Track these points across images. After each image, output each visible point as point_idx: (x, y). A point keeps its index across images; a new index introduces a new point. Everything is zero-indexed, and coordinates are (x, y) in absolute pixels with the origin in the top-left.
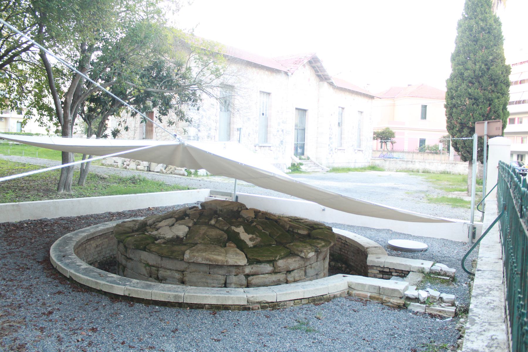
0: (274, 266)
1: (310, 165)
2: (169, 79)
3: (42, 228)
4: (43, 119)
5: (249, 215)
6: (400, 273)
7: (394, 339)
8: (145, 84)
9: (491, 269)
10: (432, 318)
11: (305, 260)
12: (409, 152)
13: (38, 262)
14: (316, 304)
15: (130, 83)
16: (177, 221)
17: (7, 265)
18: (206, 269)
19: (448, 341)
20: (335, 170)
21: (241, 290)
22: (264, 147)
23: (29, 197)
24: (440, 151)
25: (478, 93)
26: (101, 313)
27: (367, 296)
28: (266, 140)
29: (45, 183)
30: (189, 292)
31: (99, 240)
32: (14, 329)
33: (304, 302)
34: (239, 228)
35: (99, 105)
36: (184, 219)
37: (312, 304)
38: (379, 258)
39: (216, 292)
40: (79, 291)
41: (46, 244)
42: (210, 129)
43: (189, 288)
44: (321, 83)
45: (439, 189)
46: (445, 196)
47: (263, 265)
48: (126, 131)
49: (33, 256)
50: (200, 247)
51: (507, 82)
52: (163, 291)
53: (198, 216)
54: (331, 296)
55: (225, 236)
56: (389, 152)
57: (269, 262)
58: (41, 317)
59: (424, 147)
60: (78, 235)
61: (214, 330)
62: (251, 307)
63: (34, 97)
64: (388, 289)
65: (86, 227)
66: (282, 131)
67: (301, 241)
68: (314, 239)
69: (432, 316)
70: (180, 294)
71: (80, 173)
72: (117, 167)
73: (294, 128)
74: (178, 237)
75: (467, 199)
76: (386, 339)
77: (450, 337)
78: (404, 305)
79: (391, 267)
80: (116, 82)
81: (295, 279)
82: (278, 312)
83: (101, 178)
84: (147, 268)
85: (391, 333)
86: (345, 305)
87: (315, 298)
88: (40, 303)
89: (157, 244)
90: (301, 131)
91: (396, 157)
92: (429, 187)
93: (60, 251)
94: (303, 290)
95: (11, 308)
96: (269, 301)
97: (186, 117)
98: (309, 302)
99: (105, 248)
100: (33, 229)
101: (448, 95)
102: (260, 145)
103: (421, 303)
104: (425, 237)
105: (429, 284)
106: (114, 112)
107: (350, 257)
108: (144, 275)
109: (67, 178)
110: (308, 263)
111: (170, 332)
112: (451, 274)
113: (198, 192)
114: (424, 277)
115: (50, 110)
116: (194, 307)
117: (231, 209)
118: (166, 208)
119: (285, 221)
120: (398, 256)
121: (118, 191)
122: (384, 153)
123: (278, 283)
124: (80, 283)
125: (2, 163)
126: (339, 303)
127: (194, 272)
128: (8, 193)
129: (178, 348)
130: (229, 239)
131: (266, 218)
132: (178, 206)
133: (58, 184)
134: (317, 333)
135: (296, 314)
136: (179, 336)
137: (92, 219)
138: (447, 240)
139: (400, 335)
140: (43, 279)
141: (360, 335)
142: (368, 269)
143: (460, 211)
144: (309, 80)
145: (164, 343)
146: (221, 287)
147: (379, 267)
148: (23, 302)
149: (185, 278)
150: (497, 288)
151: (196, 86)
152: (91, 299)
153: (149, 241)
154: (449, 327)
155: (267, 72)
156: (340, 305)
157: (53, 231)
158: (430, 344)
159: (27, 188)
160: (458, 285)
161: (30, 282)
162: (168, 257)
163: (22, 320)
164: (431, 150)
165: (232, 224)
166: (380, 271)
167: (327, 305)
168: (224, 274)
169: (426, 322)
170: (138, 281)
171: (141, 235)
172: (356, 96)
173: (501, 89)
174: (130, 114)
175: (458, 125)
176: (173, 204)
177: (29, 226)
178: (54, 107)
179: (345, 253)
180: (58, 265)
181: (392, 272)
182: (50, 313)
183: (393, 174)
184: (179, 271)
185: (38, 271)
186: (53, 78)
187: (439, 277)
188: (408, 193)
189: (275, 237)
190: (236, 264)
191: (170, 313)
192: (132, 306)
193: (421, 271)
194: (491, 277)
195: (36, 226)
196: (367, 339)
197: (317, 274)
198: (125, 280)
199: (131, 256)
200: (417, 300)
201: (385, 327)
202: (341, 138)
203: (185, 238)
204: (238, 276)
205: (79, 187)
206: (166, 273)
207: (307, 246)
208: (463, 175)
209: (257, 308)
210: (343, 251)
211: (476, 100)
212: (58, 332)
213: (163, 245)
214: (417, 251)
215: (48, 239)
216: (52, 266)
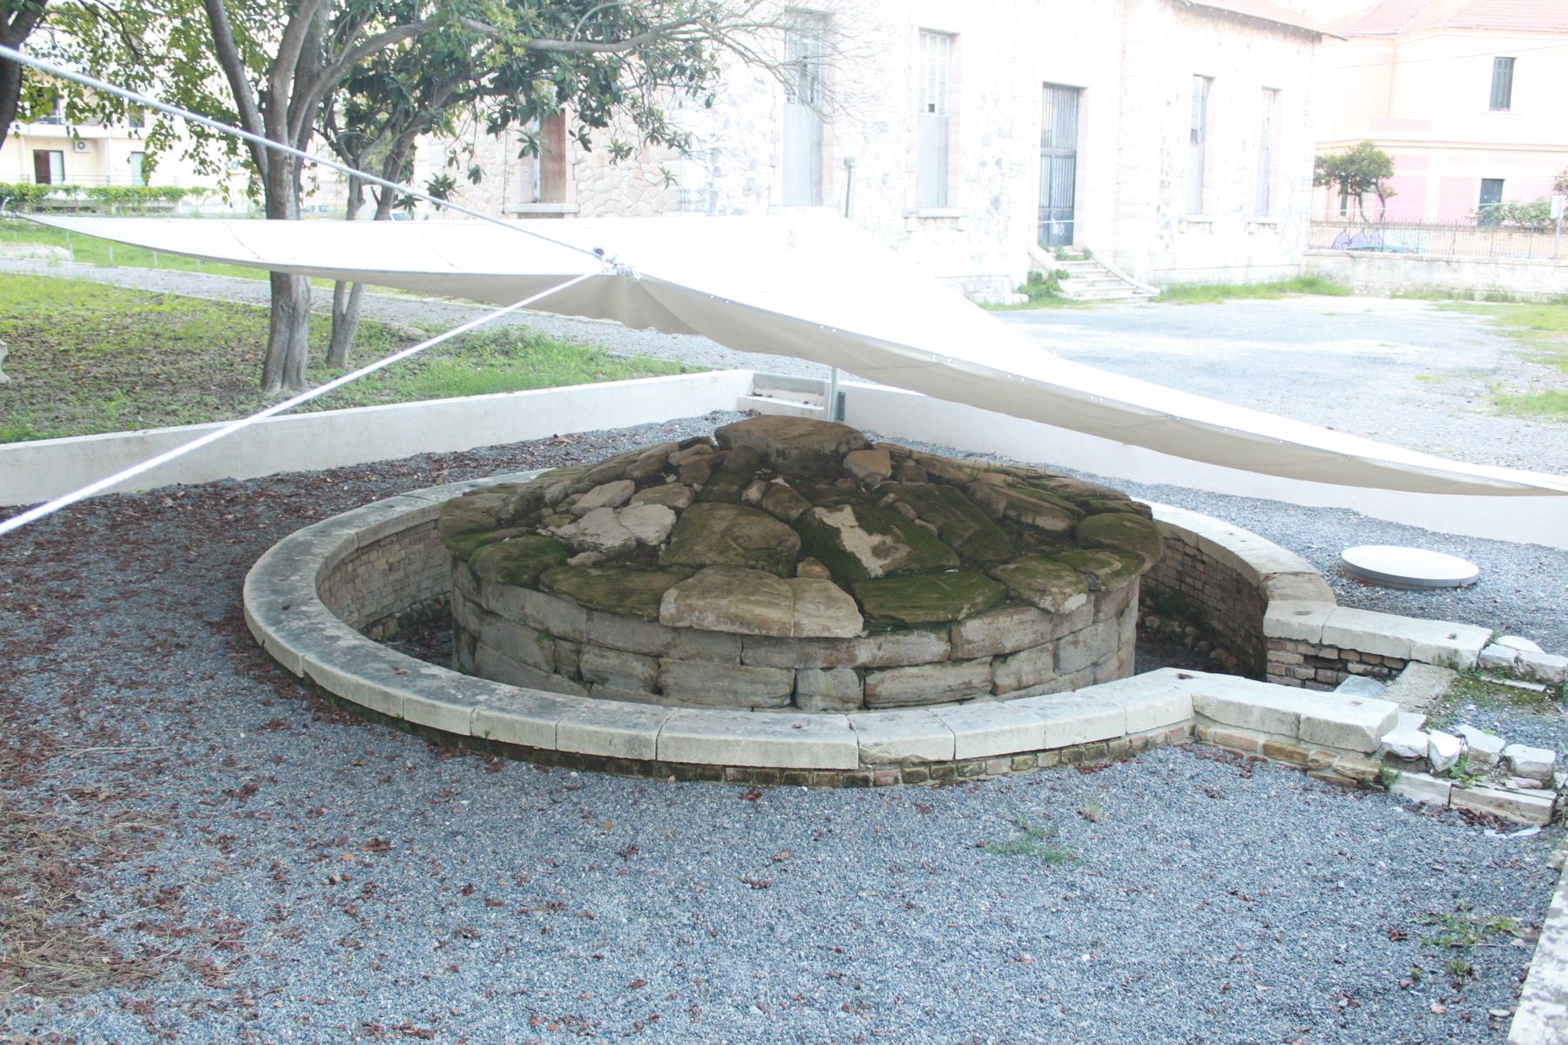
0: (950, 640)
1: (1091, 278)
3: (219, 511)
4: (206, 150)
5: (872, 469)
6: (1375, 665)
8: (526, 24)
10: (1472, 824)
11: (1055, 618)
12: (1438, 227)
13: (210, 624)
14: (1085, 768)
15: (479, 25)
16: (638, 489)
17: (117, 636)
18: (731, 648)
19: (1519, 908)
20: (1177, 293)
21: (841, 720)
22: (935, 218)
23: (174, 412)
24: (1553, 221)
26: (400, 792)
27: (1255, 743)
28: (943, 200)
29: (224, 360)
30: (673, 728)
31: (397, 547)
32: (144, 841)
33: (1043, 760)
34: (838, 514)
35: (383, 100)
36: (662, 482)
37: (1070, 767)
38: (1307, 613)
39: (758, 728)
40: (333, 721)
41: (232, 563)
42: (752, 167)
43: (675, 712)
45: (1540, 362)
47: (914, 637)
48: (475, 182)
49: (193, 603)
50: (712, 576)
52: (591, 723)
53: (708, 472)
54: (1134, 743)
55: (794, 540)
56: (1370, 226)
57: (935, 626)
58: (222, 803)
59: (1498, 209)
60: (329, 535)
61: (750, 852)
62: (871, 775)
64: (1328, 724)
66: (998, 163)
67: (1046, 557)
69: (1471, 818)
70: (645, 734)
73: (1038, 150)
74: (641, 544)
76: (1308, 892)
77: (1525, 894)
78: (1379, 779)
81: (1020, 681)
83: (401, 340)
84: (546, 643)
85: (1327, 873)
88: (217, 759)
89: (575, 567)
91: (1396, 244)
92: (1504, 353)
93: (275, 591)
94: (1042, 723)
96: (931, 756)
97: (670, 130)
98: (1060, 762)
99: (416, 573)
100: (193, 514)
102: (923, 213)
103: (1436, 775)
104: (1472, 539)
105: (1472, 707)
107: (1210, 603)
108: (537, 666)
109: (289, 346)
110: (1064, 630)
111: (613, 856)
112: (1551, 675)
113: (715, 380)
114: (1454, 684)
116: (691, 775)
117: (816, 447)
118: (612, 437)
119: (992, 486)
120: (1372, 606)
122: (1353, 232)
123: (962, 697)
124: (335, 696)
125: (93, 295)
126: (1160, 767)
127: (693, 657)
128: (110, 399)
129: (636, 909)
130: (807, 551)
131: (931, 478)
132: (650, 427)
134: (1081, 869)
136: (639, 871)
137: (374, 479)
138: (1550, 549)
140: (225, 680)
141: (1221, 879)
145: (592, 890)
146: (780, 707)
147: (1306, 642)
148: (168, 755)
151: (698, 26)
152: (370, 748)
153: (549, 559)
154: (1527, 860)
156: (1164, 772)
157: (251, 521)
158: (1455, 915)
163: (167, 813)
164: (1519, 220)
165: (815, 498)
166: (1306, 656)
167: (1121, 772)
168: (790, 664)
169: (1449, 839)
170: (514, 689)
171: (522, 540)
172: (1255, 33)
174: (484, 125)
177: (181, 506)
179: (1194, 587)
181: (1347, 661)
182: (249, 791)
183: (1381, 306)
184: (645, 655)
185: (212, 655)
187: (1508, 682)
188: (1426, 379)
189: (957, 544)
190: (826, 634)
191: (613, 792)
192: (497, 770)
193: (1449, 662)
195: (202, 506)
196: (1243, 891)
197: (1095, 664)
199: (494, 605)
200: (1422, 763)
201: (1309, 852)
203: (663, 546)
204: (834, 672)
206: (604, 661)
209: (890, 780)
210: (1189, 580)
212: (273, 852)
213: (594, 572)
214: (1441, 588)
215: (238, 549)
216: (252, 638)
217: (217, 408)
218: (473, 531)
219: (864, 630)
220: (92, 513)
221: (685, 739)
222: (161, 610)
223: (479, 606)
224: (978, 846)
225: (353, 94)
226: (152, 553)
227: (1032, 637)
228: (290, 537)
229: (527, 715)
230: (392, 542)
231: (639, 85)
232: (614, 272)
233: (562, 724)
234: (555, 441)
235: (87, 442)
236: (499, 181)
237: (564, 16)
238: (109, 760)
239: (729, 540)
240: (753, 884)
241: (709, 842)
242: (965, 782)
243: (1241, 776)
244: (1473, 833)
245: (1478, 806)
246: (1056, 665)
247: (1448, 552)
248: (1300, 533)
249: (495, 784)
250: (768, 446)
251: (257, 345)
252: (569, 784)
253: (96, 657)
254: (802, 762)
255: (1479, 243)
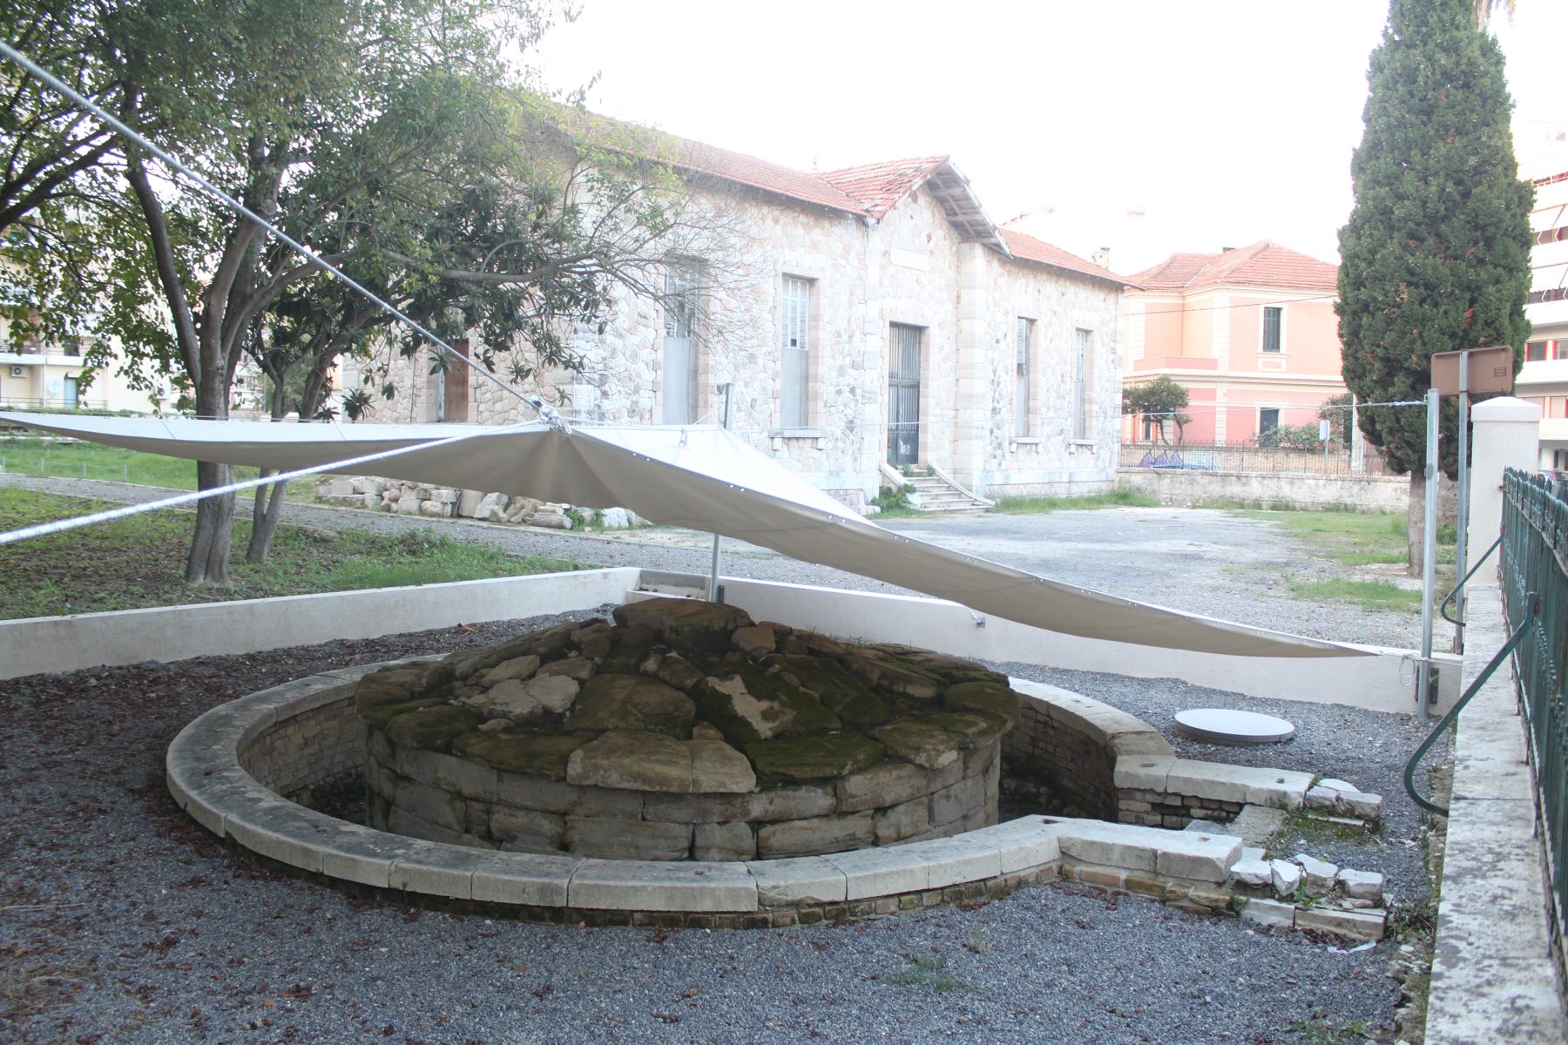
0: (835, 794)
1: (935, 492)
2: (514, 241)
3: (142, 690)
4: (141, 367)
6: (1214, 810)
7: (1204, 1009)
9: (1496, 794)
10: (1316, 942)
12: (1228, 449)
13: (132, 791)
14: (966, 906)
15: (398, 256)
16: (543, 661)
17: (39, 802)
18: (633, 805)
20: (1011, 505)
21: (741, 867)
22: (797, 439)
25: (1435, 269)
26: (320, 942)
30: (583, 876)
31: (312, 722)
32: (61, 993)
33: (927, 900)
34: (728, 683)
35: (307, 322)
36: (565, 656)
38: (1152, 765)
39: (663, 875)
40: (254, 878)
41: (154, 736)
42: (636, 391)
43: (583, 862)
44: (965, 246)
46: (1342, 576)
47: (802, 792)
48: (388, 398)
49: (116, 772)
50: (614, 739)
51: (1521, 235)
55: (690, 706)
57: (821, 782)
58: (143, 955)
59: (1275, 433)
61: (660, 988)
62: (770, 916)
63: (113, 302)
64: (1182, 858)
65: (272, 684)
66: (852, 391)
68: (955, 710)
69: (1315, 937)
70: (556, 881)
71: (251, 525)
72: (363, 505)
74: (547, 712)
75: (1408, 585)
76: (1179, 1008)
78: (1231, 905)
79: (1188, 792)
80: (354, 253)
81: (899, 832)
82: (851, 930)
83: (315, 540)
84: (458, 804)
85: (1194, 990)
86: (1054, 909)
87: (963, 888)
88: (139, 914)
89: (486, 733)
90: (908, 391)
93: (198, 759)
95: (53, 931)
96: (826, 898)
97: (566, 354)
98: (943, 901)
100: (117, 692)
101: (1347, 275)
102: (787, 434)
103: (1281, 899)
104: (1285, 701)
105: (1302, 841)
106: (352, 341)
108: (449, 827)
110: (937, 785)
112: (1368, 811)
113: (606, 576)
114: (1286, 822)
115: (160, 339)
116: (599, 920)
117: (706, 624)
118: (512, 625)
119: (866, 659)
120: (1207, 758)
121: (367, 576)
123: (849, 845)
124: (256, 854)
125: (23, 501)
127: (598, 814)
131: (811, 651)
133: (189, 559)
134: (970, 995)
135: (905, 937)
136: (555, 1009)
139: (1219, 997)
140: (147, 841)
141: (1100, 999)
142: (1118, 799)
143: (1390, 622)
144: (929, 238)
145: (510, 1028)
147: (1152, 791)
148: (89, 911)
149: (570, 834)
150: (1519, 851)
151: (594, 261)
152: (290, 901)
155: (803, 218)
156: (1038, 908)
157: (174, 699)
159: (96, 572)
160: (1391, 843)
161: (110, 852)
162: (519, 772)
163: (85, 966)
165: (708, 669)
166: (1153, 804)
167: (998, 908)
170: (430, 844)
172: (1068, 283)
173: (1506, 255)
174: (398, 347)
175: (1377, 365)
176: (529, 615)
177: (104, 685)
178: (171, 329)
179: (1047, 751)
180: (191, 799)
182: (170, 943)
184: (552, 813)
186: (167, 244)
187: (1332, 819)
190: (722, 790)
191: (527, 938)
192: (414, 920)
193: (1278, 802)
194: (1499, 819)
196: (1120, 1009)
197: (965, 817)
198: (393, 841)
199: (409, 770)
200: (1267, 888)
202: (1028, 411)
203: (568, 713)
205: (251, 566)
206: (513, 820)
207: (936, 733)
208: (1393, 513)
209: (787, 920)
210: (1042, 744)
211: (1429, 289)
213: (504, 737)
214: (1263, 743)
215: (160, 724)
216: (174, 803)
217: (143, 597)
218: (388, 702)
219: (757, 786)
220: (17, 691)
221: (595, 886)
222: (84, 778)
223: (394, 771)
224: (873, 978)
225: (280, 316)
226: (76, 728)
227: (909, 791)
228: (212, 711)
229: (443, 867)
230: (308, 718)
231: (539, 315)
232: (546, 428)
233: (476, 874)
234: (459, 629)
235: (16, 625)
236: (406, 403)
237: (473, 251)
238: (27, 917)
239: (630, 707)
240: (664, 1017)
241: (621, 981)
242: (857, 921)
243: (1107, 908)
244: (1318, 950)
245: (1319, 926)
246: (931, 818)
247: (1267, 713)
248: (1136, 700)
249: (412, 932)
250: (662, 624)
251: (181, 544)
252: (484, 932)
253: (16, 822)
254: (706, 906)
255: (1262, 461)
